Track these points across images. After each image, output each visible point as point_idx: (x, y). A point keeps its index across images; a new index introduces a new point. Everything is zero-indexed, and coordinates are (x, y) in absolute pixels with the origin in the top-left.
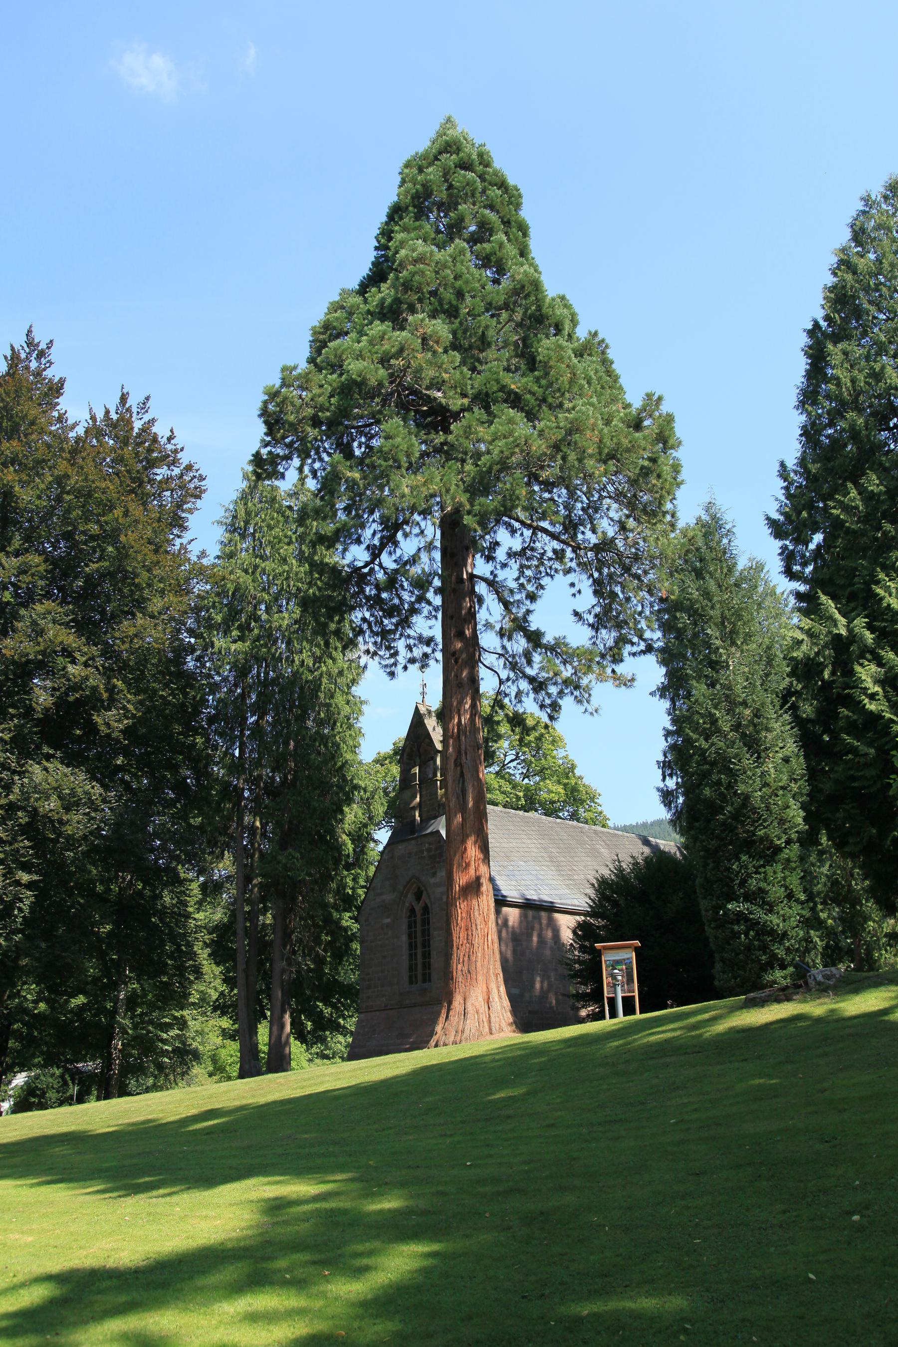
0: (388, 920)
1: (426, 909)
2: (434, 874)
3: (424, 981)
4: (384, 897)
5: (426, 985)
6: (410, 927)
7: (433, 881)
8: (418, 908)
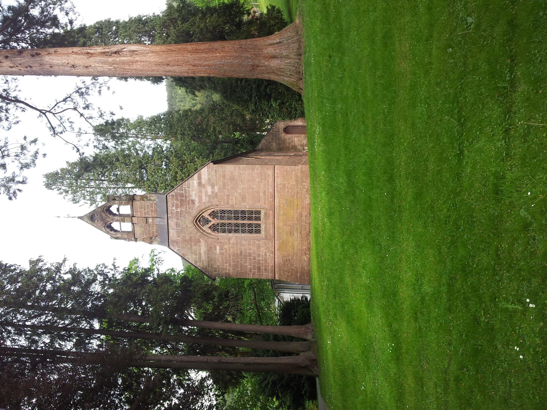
0: (218, 248)
1: (214, 214)
2: (193, 202)
3: (258, 219)
4: (202, 252)
5: (262, 215)
6: (224, 232)
7: (197, 204)
8: (214, 221)
